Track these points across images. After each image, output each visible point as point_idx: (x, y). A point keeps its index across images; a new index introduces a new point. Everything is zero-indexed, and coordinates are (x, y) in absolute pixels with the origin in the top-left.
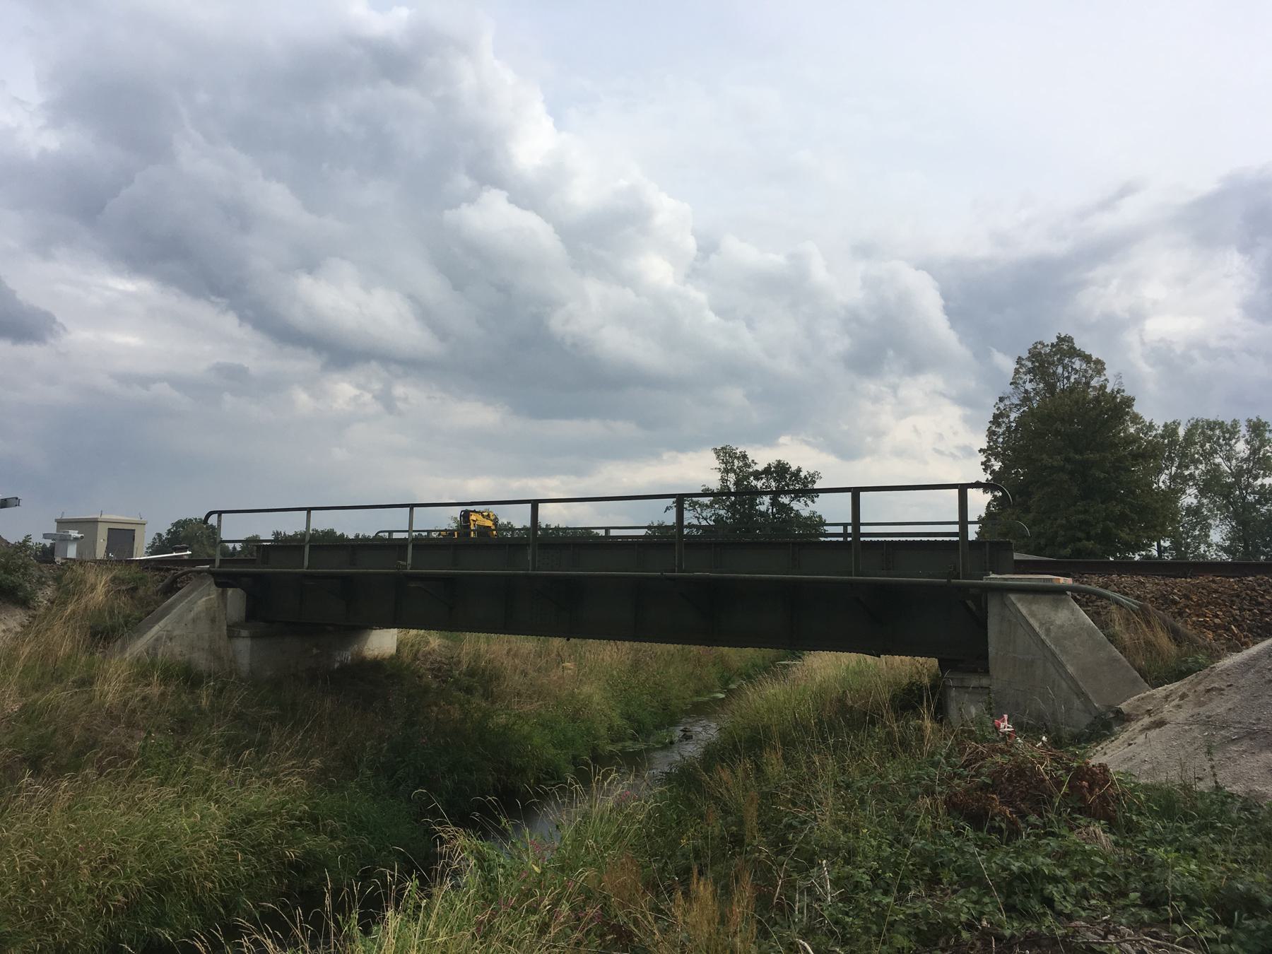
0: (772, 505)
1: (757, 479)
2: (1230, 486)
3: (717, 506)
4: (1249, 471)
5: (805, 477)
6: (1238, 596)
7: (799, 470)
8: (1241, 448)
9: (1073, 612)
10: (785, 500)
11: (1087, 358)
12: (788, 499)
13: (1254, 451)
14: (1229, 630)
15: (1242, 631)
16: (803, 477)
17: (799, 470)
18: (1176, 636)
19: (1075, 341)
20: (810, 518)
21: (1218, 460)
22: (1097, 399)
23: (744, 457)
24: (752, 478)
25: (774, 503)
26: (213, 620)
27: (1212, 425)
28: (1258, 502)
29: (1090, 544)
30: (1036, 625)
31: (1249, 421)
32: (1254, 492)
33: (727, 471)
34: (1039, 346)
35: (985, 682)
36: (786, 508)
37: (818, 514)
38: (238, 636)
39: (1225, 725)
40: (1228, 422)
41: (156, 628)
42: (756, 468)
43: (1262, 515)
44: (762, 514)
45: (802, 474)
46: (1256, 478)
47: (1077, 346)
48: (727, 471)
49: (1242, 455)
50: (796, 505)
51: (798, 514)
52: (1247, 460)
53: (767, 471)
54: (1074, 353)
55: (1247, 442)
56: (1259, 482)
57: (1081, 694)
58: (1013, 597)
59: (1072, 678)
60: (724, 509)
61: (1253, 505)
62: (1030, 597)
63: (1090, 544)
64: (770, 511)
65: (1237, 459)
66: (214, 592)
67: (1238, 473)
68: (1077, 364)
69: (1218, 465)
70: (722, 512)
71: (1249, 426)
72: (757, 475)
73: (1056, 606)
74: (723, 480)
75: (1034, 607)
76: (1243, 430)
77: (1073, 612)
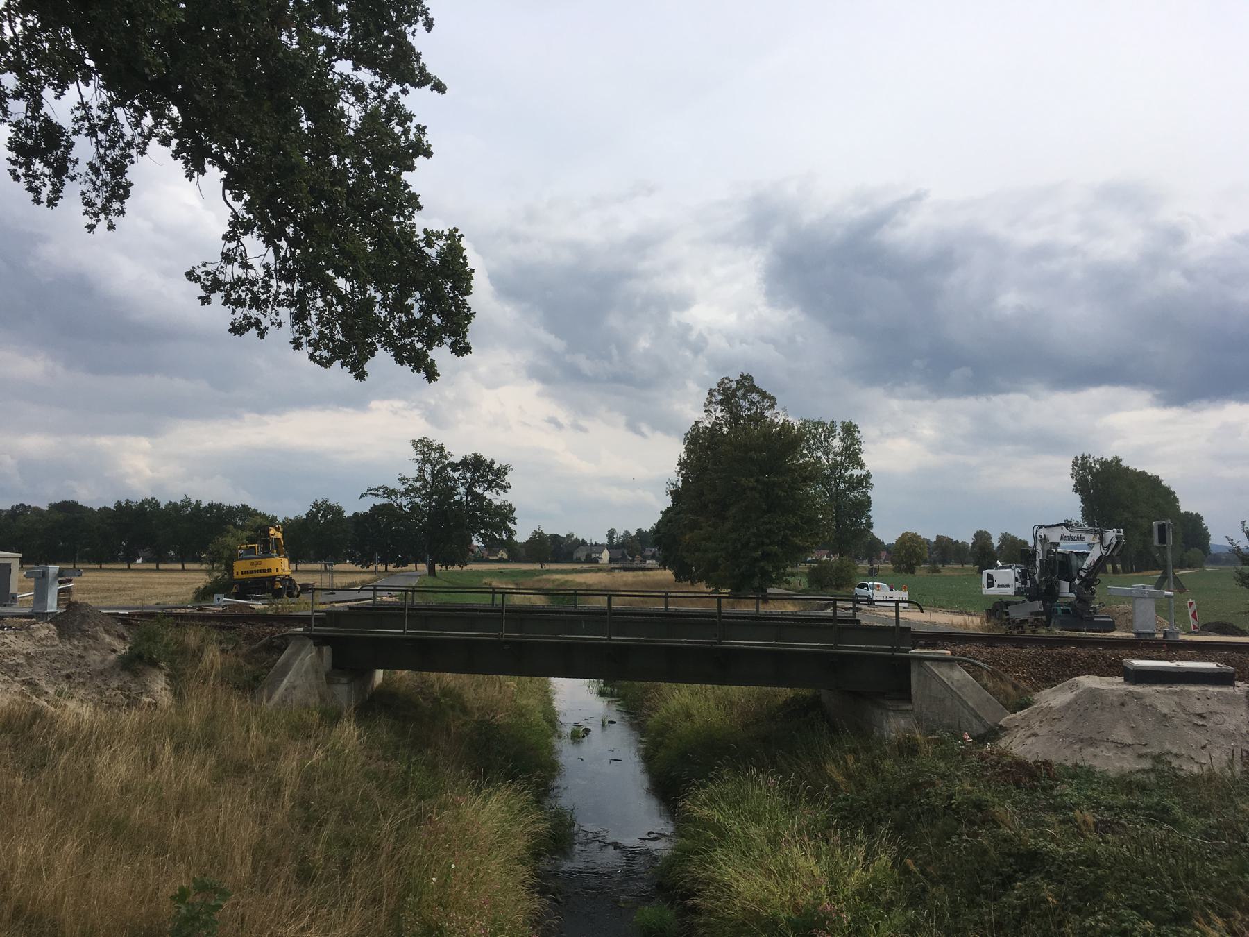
0: (467, 494)
1: (454, 470)
2: (828, 477)
3: (412, 494)
4: (842, 464)
5: (498, 469)
6: (1030, 661)
7: (492, 463)
8: (836, 444)
9: (960, 671)
10: (479, 490)
11: (764, 395)
12: (481, 489)
13: (846, 448)
14: (1030, 680)
15: (1036, 680)
16: (495, 469)
17: (492, 463)
18: (1015, 687)
19: (754, 379)
20: (499, 507)
21: (820, 454)
22: (779, 433)
23: (441, 449)
24: (449, 469)
25: (469, 492)
26: (317, 672)
27: (817, 425)
28: (848, 489)
29: (775, 548)
30: (945, 680)
31: (843, 423)
32: (845, 482)
33: (425, 462)
34: (726, 381)
35: (910, 707)
36: (480, 498)
37: (509, 503)
38: (339, 682)
39: (1067, 736)
40: (828, 422)
41: (285, 681)
42: (452, 459)
43: (851, 500)
44: (459, 503)
45: (496, 467)
46: (846, 470)
47: (756, 383)
48: (425, 462)
49: (837, 449)
50: (489, 495)
51: (490, 503)
52: (840, 454)
53: (464, 463)
54: (753, 389)
55: (841, 440)
56: (849, 473)
57: (977, 716)
58: (928, 663)
59: (972, 709)
60: (419, 497)
61: (844, 491)
62: (936, 663)
63: (775, 548)
64: (464, 499)
65: (833, 453)
66: (314, 650)
67: (834, 466)
68: (755, 397)
69: (820, 458)
70: (418, 500)
71: (843, 427)
72: (454, 467)
73: (951, 667)
74: (420, 470)
75: (941, 669)
76: (839, 430)
77: (960, 671)
